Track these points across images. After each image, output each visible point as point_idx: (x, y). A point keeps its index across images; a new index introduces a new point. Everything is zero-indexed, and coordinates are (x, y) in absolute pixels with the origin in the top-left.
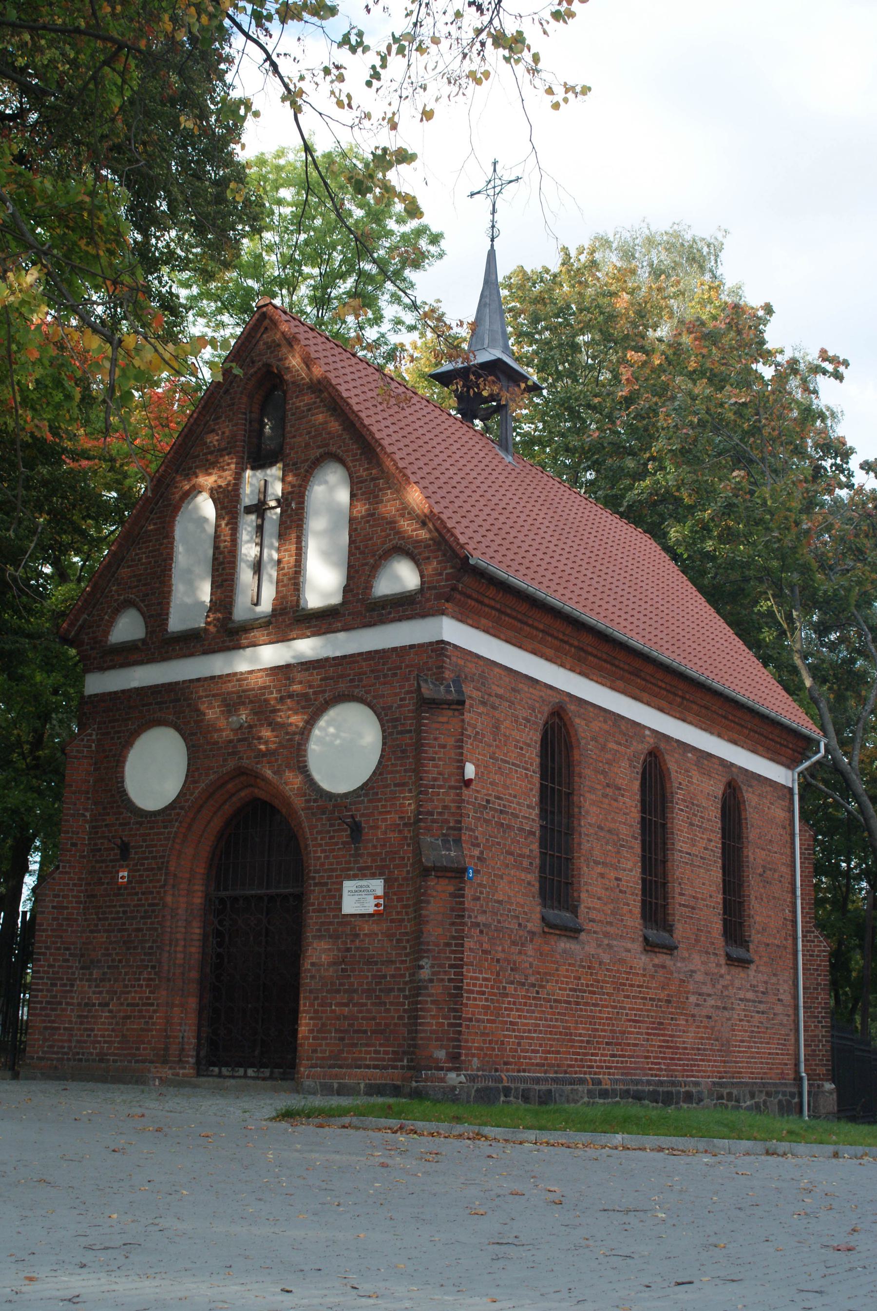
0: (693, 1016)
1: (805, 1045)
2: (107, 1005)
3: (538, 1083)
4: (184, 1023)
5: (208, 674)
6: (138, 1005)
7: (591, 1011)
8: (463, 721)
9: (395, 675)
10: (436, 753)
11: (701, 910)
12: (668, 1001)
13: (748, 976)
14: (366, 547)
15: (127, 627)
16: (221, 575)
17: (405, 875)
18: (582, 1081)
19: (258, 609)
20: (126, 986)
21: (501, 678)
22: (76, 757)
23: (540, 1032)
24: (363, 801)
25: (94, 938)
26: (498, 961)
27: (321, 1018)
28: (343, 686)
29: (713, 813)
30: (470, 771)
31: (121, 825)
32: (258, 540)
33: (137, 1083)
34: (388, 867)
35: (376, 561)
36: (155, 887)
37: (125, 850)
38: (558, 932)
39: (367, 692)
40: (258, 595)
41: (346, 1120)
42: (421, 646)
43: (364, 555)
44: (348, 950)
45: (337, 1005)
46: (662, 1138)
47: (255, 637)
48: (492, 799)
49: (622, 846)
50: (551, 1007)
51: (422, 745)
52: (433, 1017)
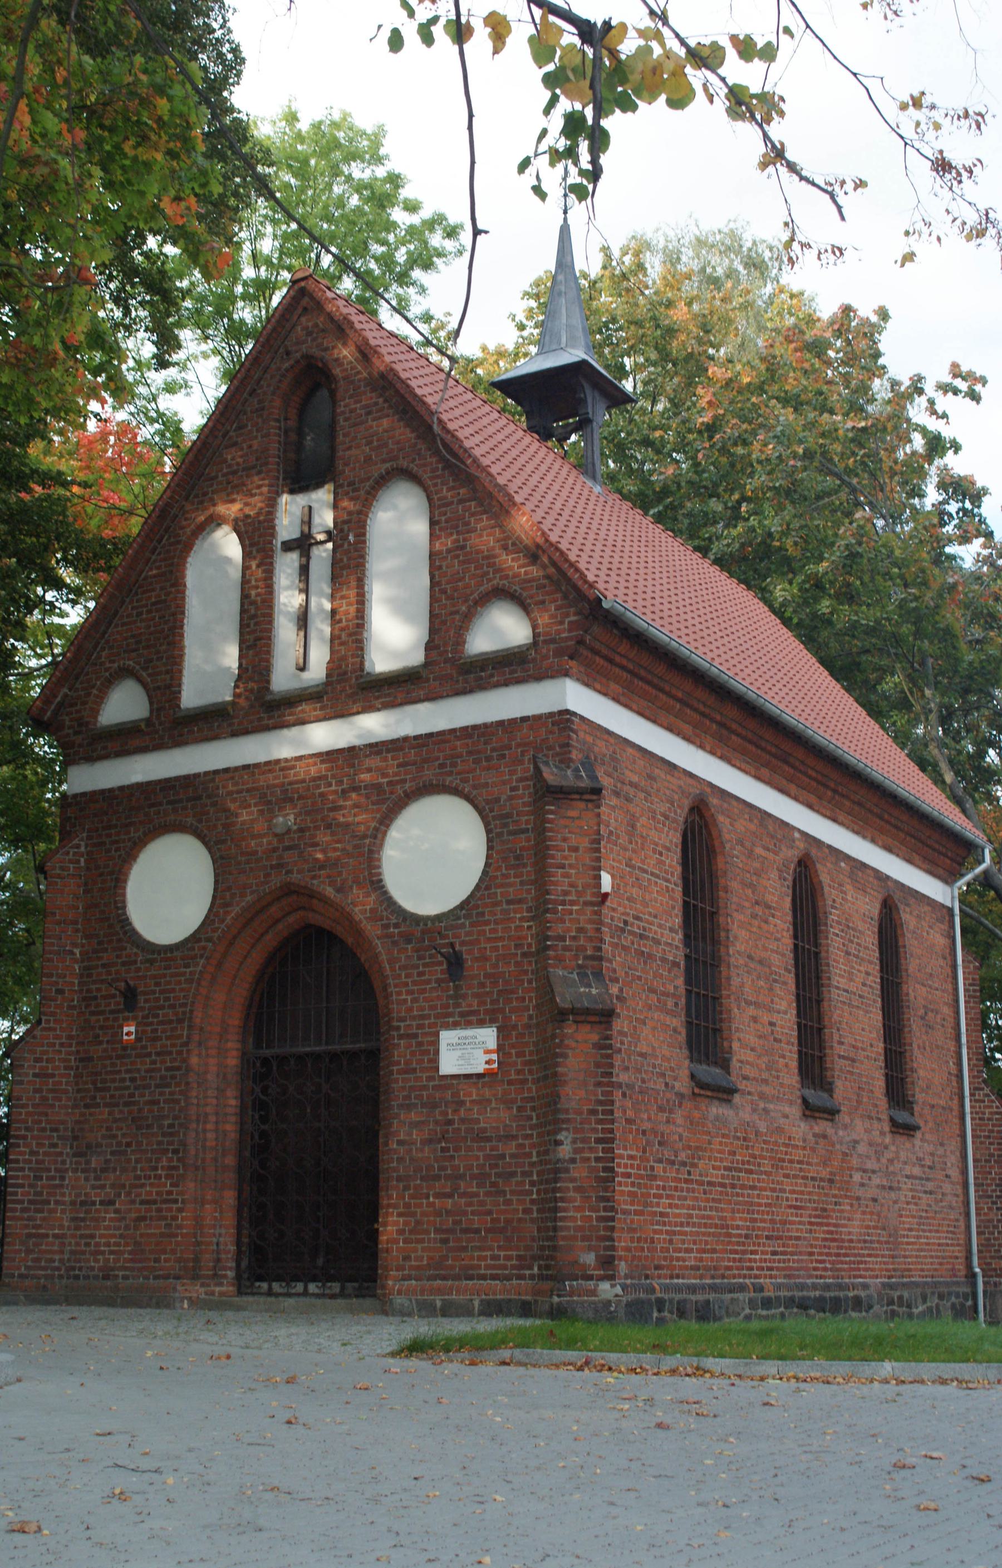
0: (858, 1199)
1: (978, 1233)
3: (694, 1292)
5: (262, 758)
6: (155, 1202)
7: (749, 1196)
8: (598, 815)
9: (503, 756)
10: (565, 858)
11: (862, 1063)
12: (831, 1181)
13: (914, 1146)
14: (455, 589)
15: (124, 704)
16: (254, 632)
17: (526, 1020)
18: (742, 1288)
19: (306, 675)
20: (139, 1178)
21: (634, 762)
22: (59, 876)
23: (694, 1225)
24: (463, 925)
26: (644, 1132)
27: (413, 1214)
28: (429, 774)
29: (870, 939)
30: (606, 882)
31: (124, 964)
32: (302, 586)
33: (158, 1306)
34: (502, 1011)
35: (469, 608)
37: (130, 997)
38: (709, 1093)
39: (465, 780)
40: (301, 657)
41: (505, 1354)
42: (537, 718)
43: (451, 602)
44: (450, 1122)
45: (437, 1196)
46: (942, 1365)
47: (303, 711)
48: (631, 920)
49: (775, 981)
50: (705, 1193)
51: (548, 848)
52: (578, 1209)
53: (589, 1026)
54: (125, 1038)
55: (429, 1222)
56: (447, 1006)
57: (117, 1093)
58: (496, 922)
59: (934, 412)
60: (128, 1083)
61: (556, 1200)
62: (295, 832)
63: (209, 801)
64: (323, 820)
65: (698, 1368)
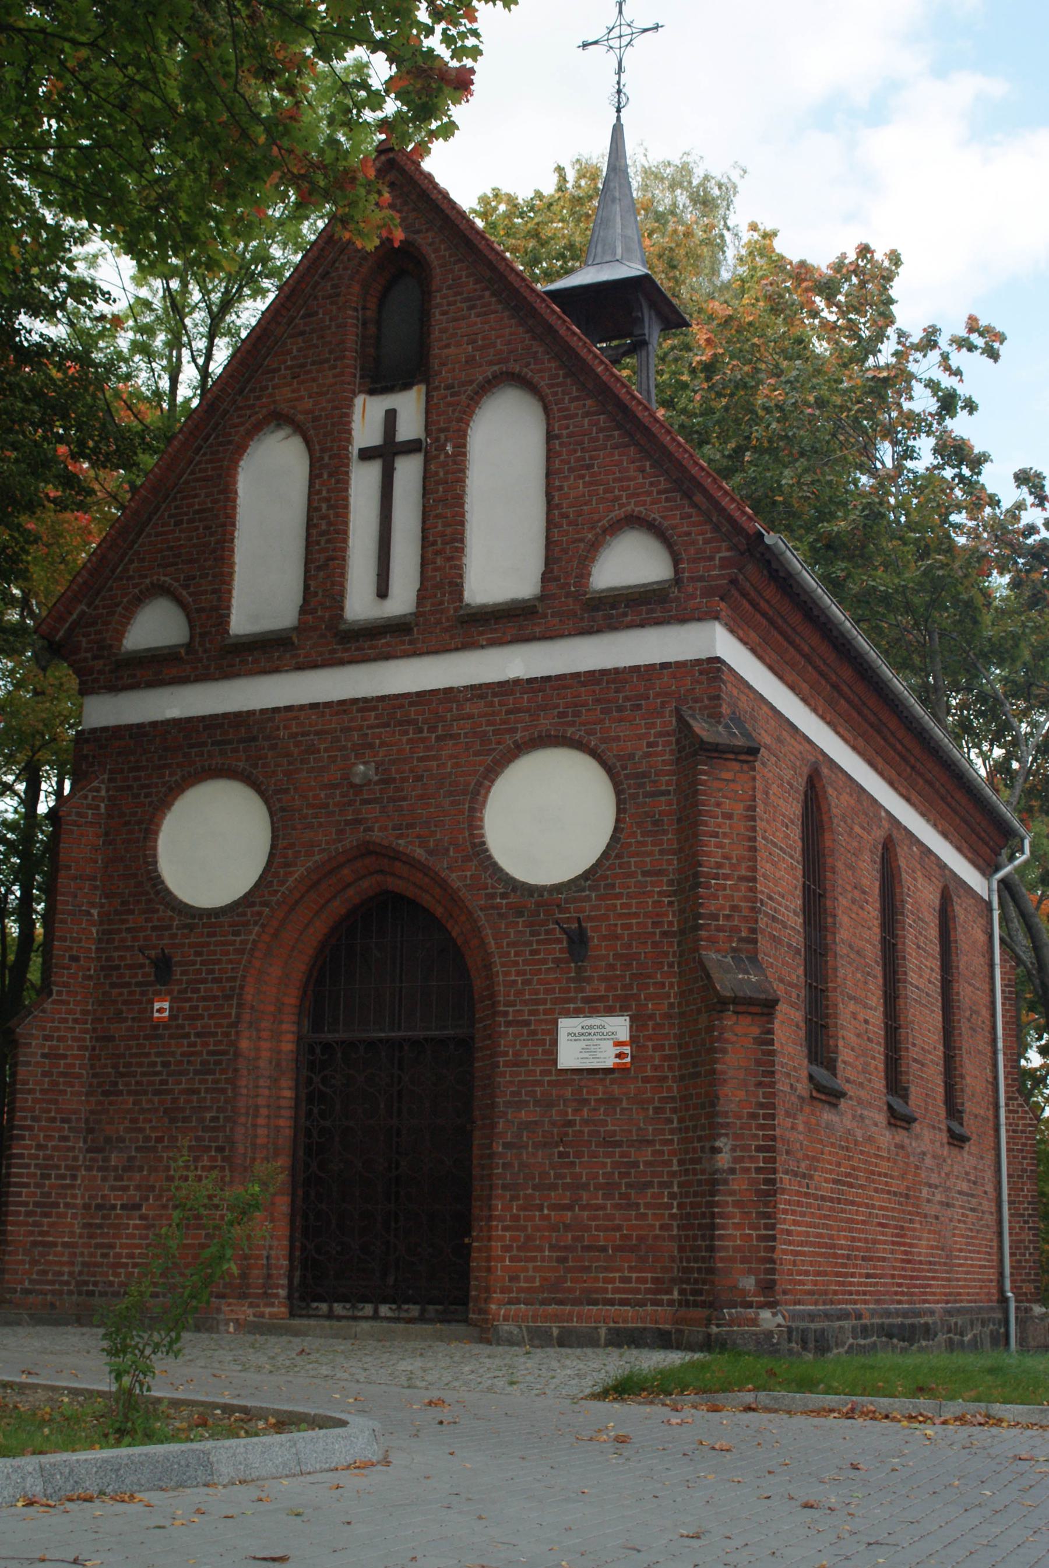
2: (139, 1207)
4: (269, 1237)
9: (639, 707)
10: (719, 826)
14: (580, 514)
15: (155, 627)
21: (767, 722)
22: (75, 823)
24: (588, 898)
25: (111, 1103)
27: (524, 1229)
28: (546, 723)
31: (154, 928)
35: (597, 535)
36: (220, 1026)
37: (163, 968)
38: (823, 1097)
39: (590, 733)
44: (570, 1123)
45: (552, 1207)
49: (868, 974)
52: (737, 1226)
53: (750, 1018)
54: (156, 1015)
55: (542, 1238)
56: (568, 990)
57: (145, 1079)
58: (629, 896)
59: (948, 368)
60: (159, 1068)
61: (713, 1215)
62: (377, 783)
63: (266, 744)
64: (411, 771)
65: (988, 1416)
